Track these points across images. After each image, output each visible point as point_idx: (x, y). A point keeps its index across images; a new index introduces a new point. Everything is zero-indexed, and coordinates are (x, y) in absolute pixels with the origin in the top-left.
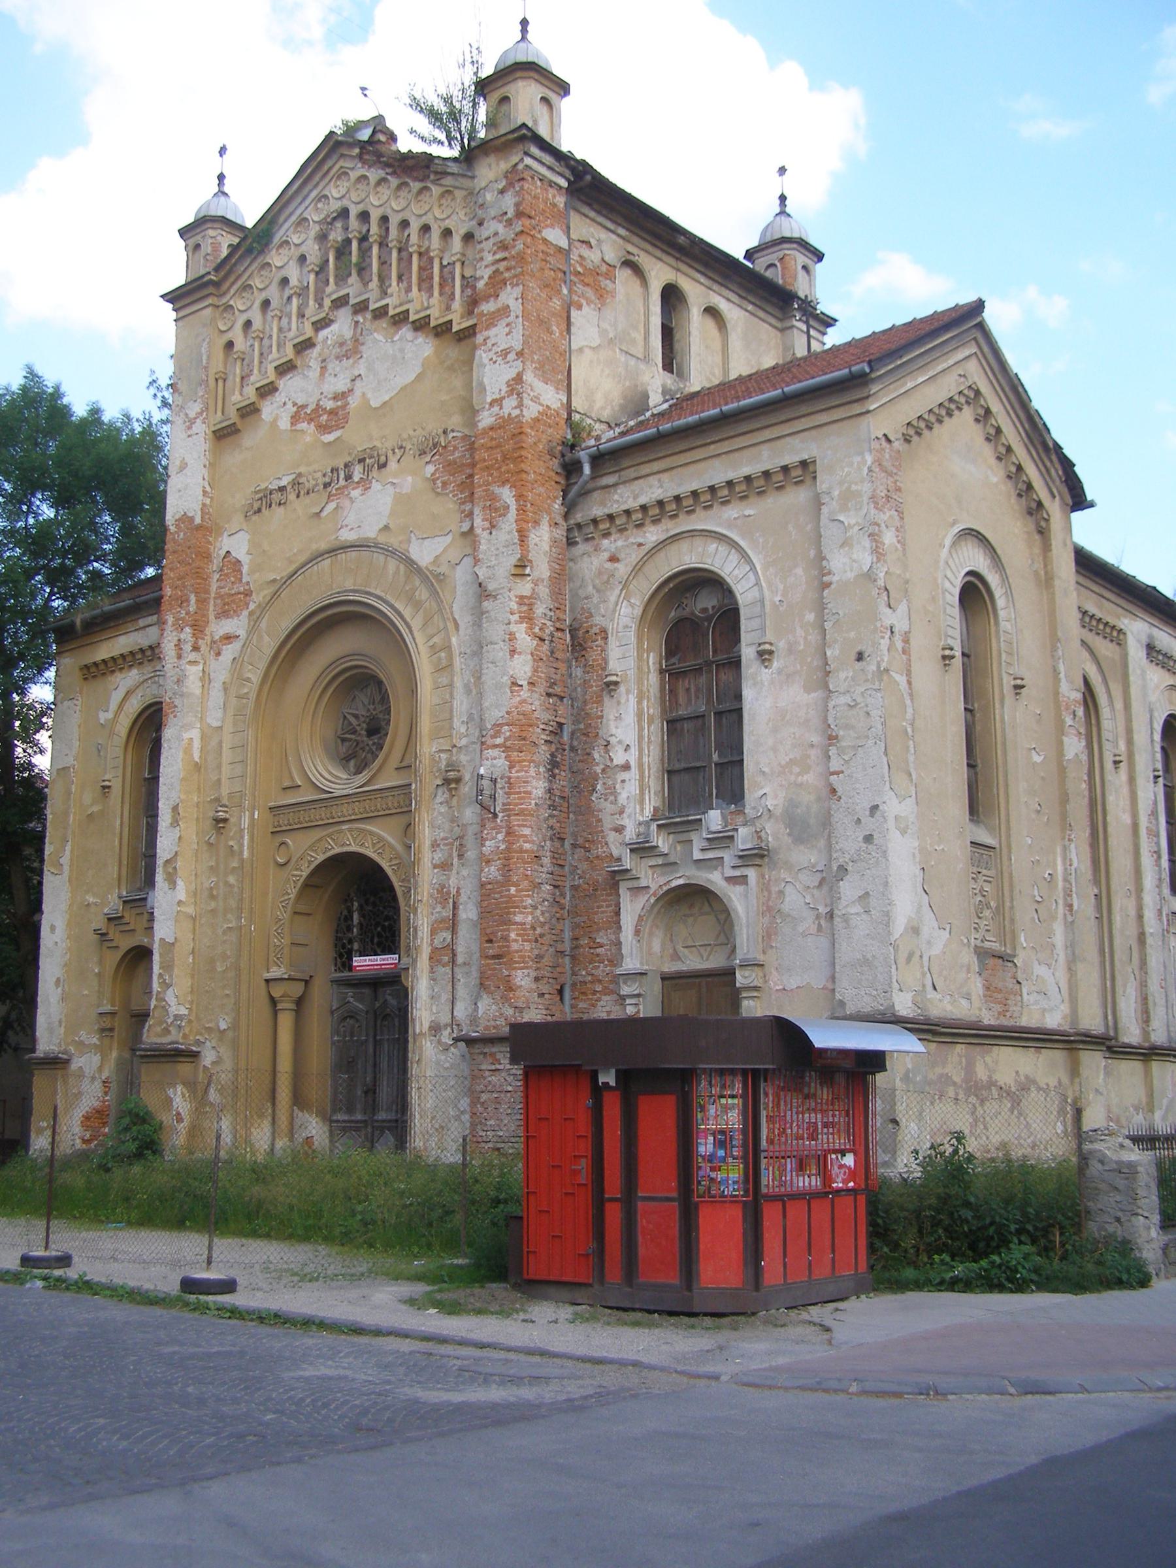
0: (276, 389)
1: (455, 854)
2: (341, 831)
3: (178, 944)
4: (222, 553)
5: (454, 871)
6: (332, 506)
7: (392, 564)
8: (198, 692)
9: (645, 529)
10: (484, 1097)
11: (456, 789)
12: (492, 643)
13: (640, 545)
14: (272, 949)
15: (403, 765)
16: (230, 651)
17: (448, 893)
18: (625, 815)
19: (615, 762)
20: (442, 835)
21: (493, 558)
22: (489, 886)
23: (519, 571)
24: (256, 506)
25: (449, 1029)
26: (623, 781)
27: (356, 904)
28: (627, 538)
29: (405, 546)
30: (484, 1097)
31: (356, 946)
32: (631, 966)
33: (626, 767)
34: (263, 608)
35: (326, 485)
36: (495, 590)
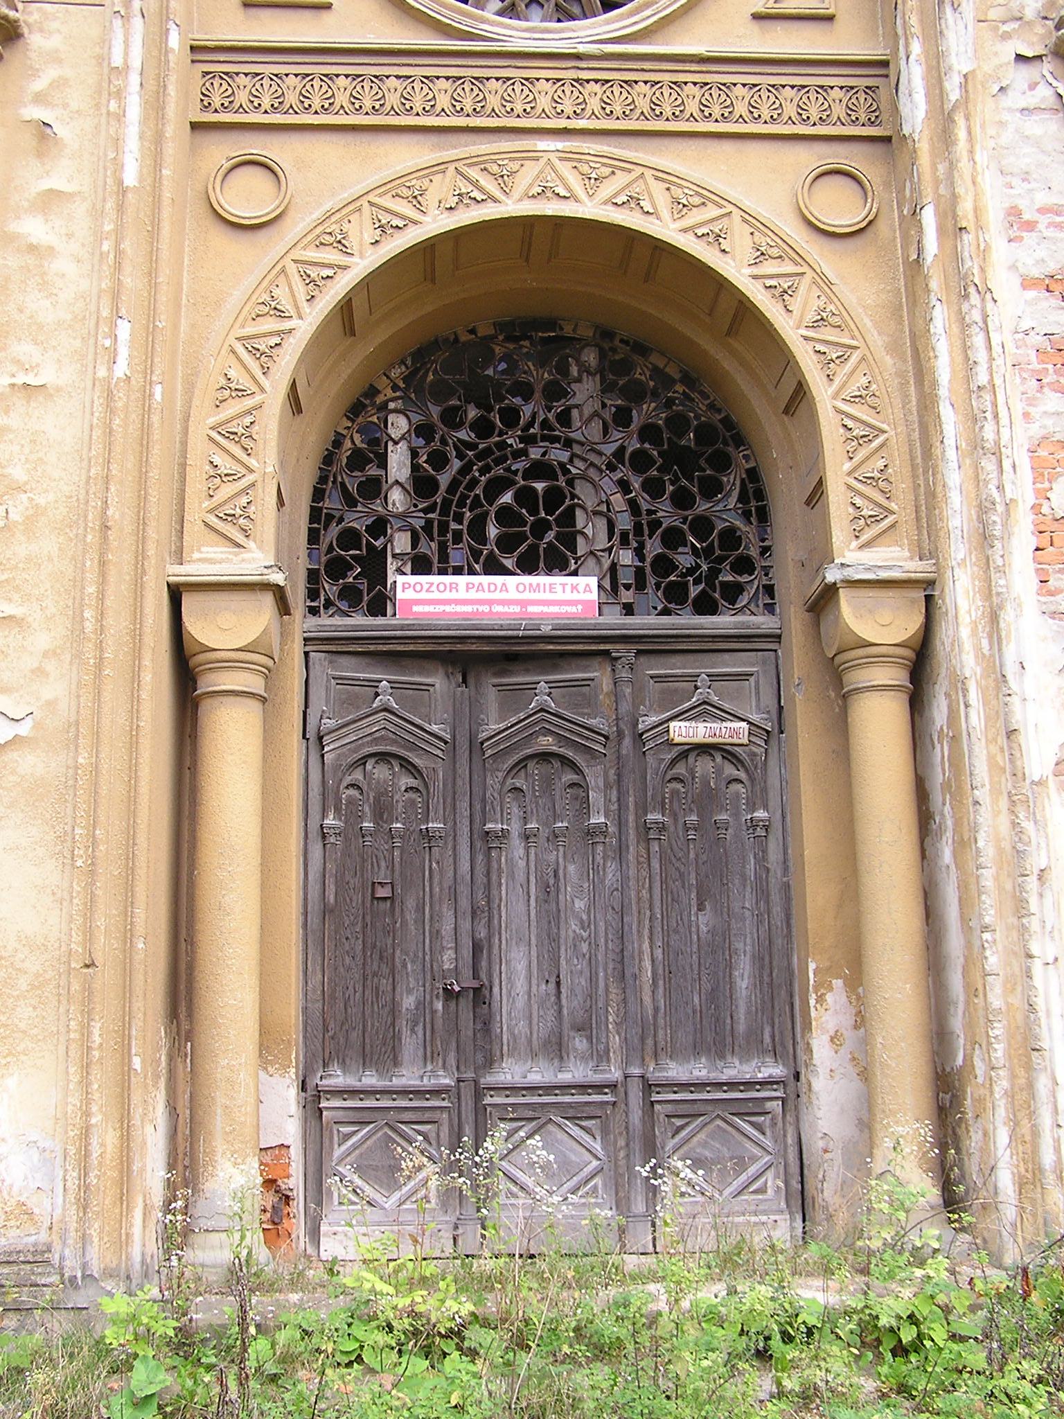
27: (399, 425)
31: (401, 542)
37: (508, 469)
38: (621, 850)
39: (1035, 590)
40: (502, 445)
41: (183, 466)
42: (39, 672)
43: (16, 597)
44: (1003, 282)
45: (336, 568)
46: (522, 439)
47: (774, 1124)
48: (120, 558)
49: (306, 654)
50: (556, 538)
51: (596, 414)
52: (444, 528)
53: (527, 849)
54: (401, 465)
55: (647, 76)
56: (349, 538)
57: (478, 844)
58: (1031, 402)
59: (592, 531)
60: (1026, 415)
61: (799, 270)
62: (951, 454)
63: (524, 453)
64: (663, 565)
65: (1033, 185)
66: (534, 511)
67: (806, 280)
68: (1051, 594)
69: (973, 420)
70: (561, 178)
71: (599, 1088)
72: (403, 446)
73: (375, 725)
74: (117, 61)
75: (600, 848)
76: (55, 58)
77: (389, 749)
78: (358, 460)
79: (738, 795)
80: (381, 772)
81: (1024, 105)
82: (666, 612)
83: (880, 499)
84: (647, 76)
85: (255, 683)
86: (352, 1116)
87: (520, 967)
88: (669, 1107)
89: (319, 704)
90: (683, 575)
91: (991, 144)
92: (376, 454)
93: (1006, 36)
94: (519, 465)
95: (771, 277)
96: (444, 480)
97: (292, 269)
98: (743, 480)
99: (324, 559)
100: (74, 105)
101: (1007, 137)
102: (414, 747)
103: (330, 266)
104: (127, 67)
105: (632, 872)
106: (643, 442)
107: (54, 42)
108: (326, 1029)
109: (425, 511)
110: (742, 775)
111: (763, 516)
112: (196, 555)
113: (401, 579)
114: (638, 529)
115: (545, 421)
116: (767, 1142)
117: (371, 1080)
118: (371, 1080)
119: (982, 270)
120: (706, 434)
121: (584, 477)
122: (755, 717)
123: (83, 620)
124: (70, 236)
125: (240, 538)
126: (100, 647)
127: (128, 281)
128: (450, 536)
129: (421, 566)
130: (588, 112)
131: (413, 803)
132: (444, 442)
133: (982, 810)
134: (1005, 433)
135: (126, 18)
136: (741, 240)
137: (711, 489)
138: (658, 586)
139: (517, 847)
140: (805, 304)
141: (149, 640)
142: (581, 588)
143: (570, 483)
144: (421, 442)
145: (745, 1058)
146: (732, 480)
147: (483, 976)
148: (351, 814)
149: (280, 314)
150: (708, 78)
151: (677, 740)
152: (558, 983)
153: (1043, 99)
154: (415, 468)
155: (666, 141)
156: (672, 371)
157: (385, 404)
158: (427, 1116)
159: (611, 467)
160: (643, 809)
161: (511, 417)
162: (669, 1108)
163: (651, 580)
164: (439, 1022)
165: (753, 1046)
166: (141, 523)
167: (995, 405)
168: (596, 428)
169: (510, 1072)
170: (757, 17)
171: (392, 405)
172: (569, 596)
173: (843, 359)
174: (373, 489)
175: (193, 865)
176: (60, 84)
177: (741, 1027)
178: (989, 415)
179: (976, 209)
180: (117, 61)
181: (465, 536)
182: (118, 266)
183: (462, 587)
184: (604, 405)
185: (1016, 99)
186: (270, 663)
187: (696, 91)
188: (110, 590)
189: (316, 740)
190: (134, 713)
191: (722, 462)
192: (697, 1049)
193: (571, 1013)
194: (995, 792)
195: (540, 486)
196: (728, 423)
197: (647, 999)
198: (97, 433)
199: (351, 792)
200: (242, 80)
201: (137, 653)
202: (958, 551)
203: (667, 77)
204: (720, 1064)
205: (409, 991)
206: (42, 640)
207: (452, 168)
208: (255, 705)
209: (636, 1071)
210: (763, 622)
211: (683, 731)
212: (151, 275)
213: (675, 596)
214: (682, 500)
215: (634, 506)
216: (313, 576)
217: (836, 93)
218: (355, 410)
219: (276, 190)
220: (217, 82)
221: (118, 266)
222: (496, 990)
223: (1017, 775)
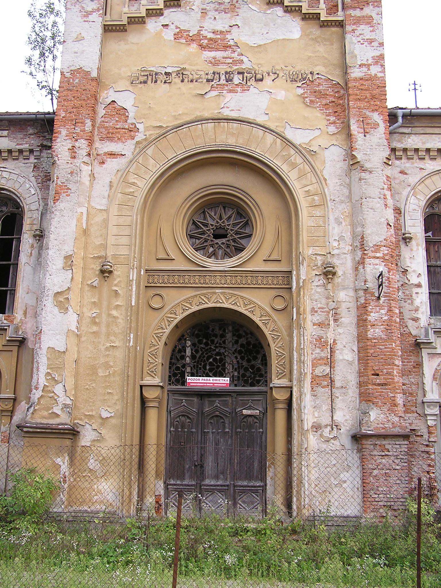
0: (162, 14)
1: (331, 319)
2: (215, 293)
3: (67, 353)
4: (109, 101)
5: (331, 329)
6: (214, 93)
7: (270, 138)
8: (87, 183)
9: (425, 161)
10: (375, 472)
11: (332, 279)
12: (370, 197)
13: (421, 169)
14: (145, 365)
15: (271, 258)
16: (112, 164)
17: (326, 342)
18: (419, 312)
19: (411, 282)
20: (319, 306)
21: (368, 150)
22: (375, 341)
23: (387, 161)
24: (142, 79)
25: (329, 428)
26: (417, 293)
27: (189, 343)
28: (413, 164)
29: (282, 130)
30: (375, 472)
31: (188, 369)
32: (432, 397)
33: (419, 286)
34: (149, 142)
35: (208, 81)
36: (371, 168)
37: (212, 354)
38: (232, 437)
39: (310, 390)
40: (211, 348)
41: (143, 360)
42: (115, 403)
43: (111, 389)
44: (309, 325)
45: (175, 375)
46: (215, 347)
47: (260, 495)
48: (131, 381)
49: (168, 394)
50: (221, 369)
51: (231, 341)
52: (197, 366)
53: (213, 435)
54: (189, 352)
55: (240, 275)
56: (178, 368)
57: (203, 434)
58: (313, 350)
59: (229, 368)
60: (312, 353)
61: (270, 318)
62: (295, 362)
63: (215, 350)
64: (244, 375)
65: (318, 302)
66: (217, 363)
67: (271, 321)
68: (314, 391)
69: (300, 355)
70: (221, 298)
71: (224, 486)
72: (189, 348)
73: (181, 409)
74: (131, 279)
75: (227, 436)
76: (119, 276)
77: (185, 414)
78: (180, 351)
79: (257, 425)
80: (183, 419)
81: (317, 285)
82: (244, 386)
83: (283, 369)
84: (240, 275)
85: (156, 404)
86: (174, 489)
87: (210, 460)
88: (239, 491)
89: (170, 404)
90: (248, 378)
91: (310, 293)
92: (184, 350)
93: (314, 270)
94: (214, 353)
95: (263, 320)
96: (198, 356)
97: (165, 318)
98: (262, 356)
99: (172, 373)
100: (122, 286)
101: (313, 292)
102: (189, 414)
103: (173, 318)
104: (133, 279)
105: (234, 441)
106: (241, 348)
107: (119, 273)
108: (170, 472)
109: (193, 363)
110: (258, 422)
111: (266, 364)
112: (145, 379)
113: (188, 378)
114: (239, 367)
115: (220, 342)
116: (258, 498)
117: (178, 482)
118: (178, 482)
119: (304, 323)
120: (255, 346)
121: (228, 356)
122: (260, 409)
123: (124, 394)
124: (121, 314)
125: (154, 376)
126: (127, 400)
127: (133, 325)
128: (199, 368)
129: (193, 375)
130: (227, 283)
131: (189, 425)
132: (198, 347)
133: (295, 436)
134: (306, 358)
135: (133, 269)
136: (258, 312)
137: (255, 358)
138: (242, 380)
139: (211, 435)
140: (270, 326)
141: (136, 398)
142: (226, 380)
143: (225, 357)
144: (193, 347)
145: (255, 481)
146: (260, 356)
147: (203, 461)
148: (176, 428)
149: (163, 329)
150: (253, 275)
151: (244, 414)
152: (218, 464)
153: (321, 284)
154: (192, 353)
155: (244, 289)
156: (248, 332)
157: (186, 338)
158: (190, 490)
159: (234, 353)
160: (236, 429)
161: (213, 342)
162: (239, 491)
163: (241, 379)
164: (193, 471)
165: (257, 479)
166: (135, 375)
167: (304, 352)
168: (231, 344)
169: (207, 482)
170: (264, 260)
171: (187, 339)
172: (223, 382)
173: (277, 338)
174: (183, 357)
175: (144, 436)
176: (120, 282)
177: (255, 474)
178: (303, 355)
179: (304, 310)
180: (131, 279)
181: (202, 368)
182: (131, 322)
183: (201, 380)
184: (233, 339)
185: (315, 284)
186: (159, 400)
187: (250, 278)
188: (129, 389)
189: (169, 412)
190: (133, 412)
191: (258, 352)
192: (246, 478)
193: (220, 470)
194: (298, 432)
195: (218, 357)
196: (260, 343)
197: (235, 467)
198: (127, 357)
199: (177, 423)
200: (156, 276)
201: (134, 400)
202: (295, 383)
203: (244, 275)
204: (250, 482)
205: (187, 464)
206: (116, 397)
207: (198, 296)
208: (159, 388)
209: (232, 483)
210: (263, 388)
211: (245, 412)
212: (137, 322)
213: (246, 383)
214: (249, 361)
215: (238, 362)
216: (170, 376)
217: (280, 278)
218: (180, 340)
219: (162, 300)
220: (151, 277)
221: (131, 322)
222: (205, 465)
223: (303, 429)
